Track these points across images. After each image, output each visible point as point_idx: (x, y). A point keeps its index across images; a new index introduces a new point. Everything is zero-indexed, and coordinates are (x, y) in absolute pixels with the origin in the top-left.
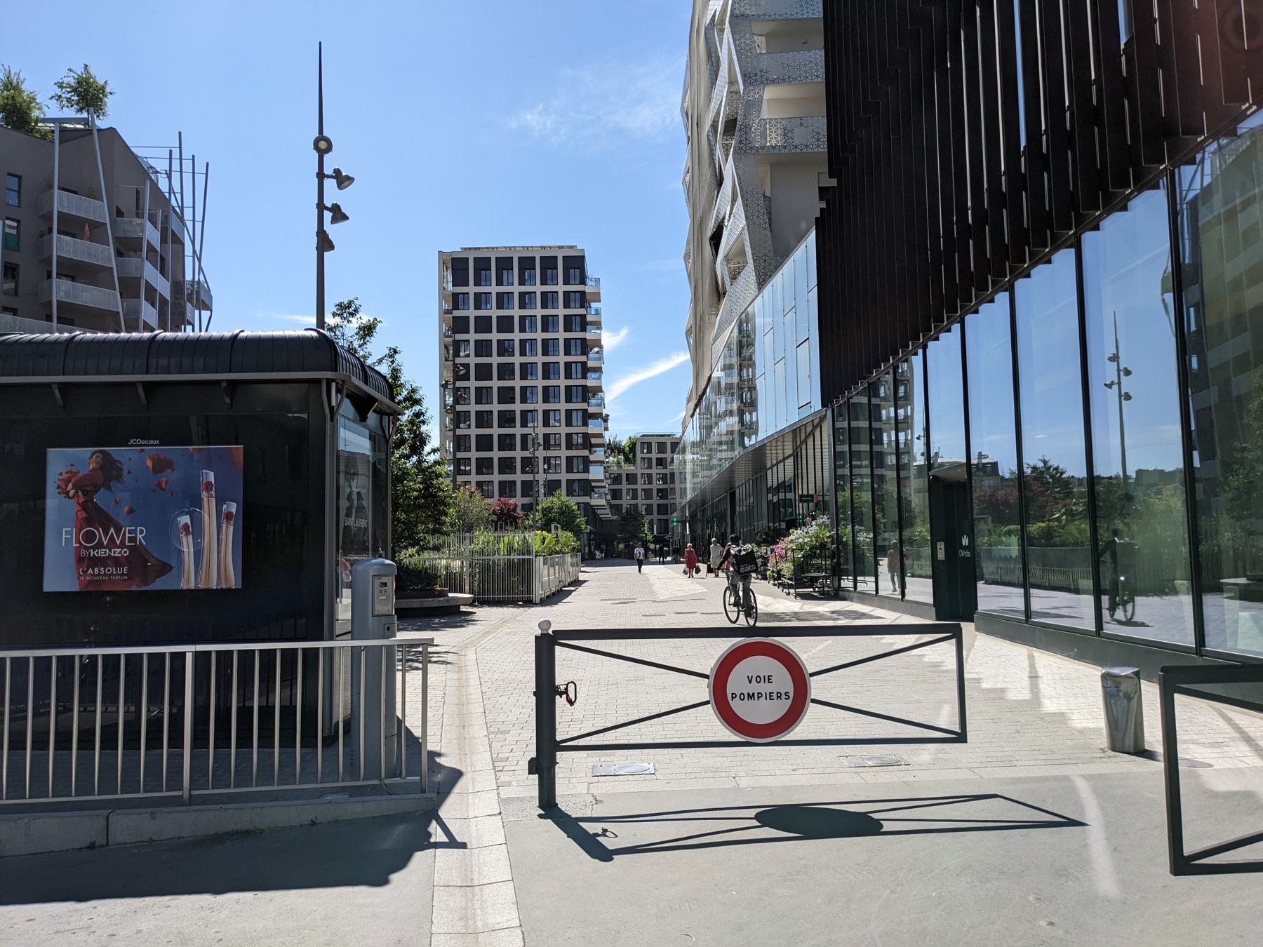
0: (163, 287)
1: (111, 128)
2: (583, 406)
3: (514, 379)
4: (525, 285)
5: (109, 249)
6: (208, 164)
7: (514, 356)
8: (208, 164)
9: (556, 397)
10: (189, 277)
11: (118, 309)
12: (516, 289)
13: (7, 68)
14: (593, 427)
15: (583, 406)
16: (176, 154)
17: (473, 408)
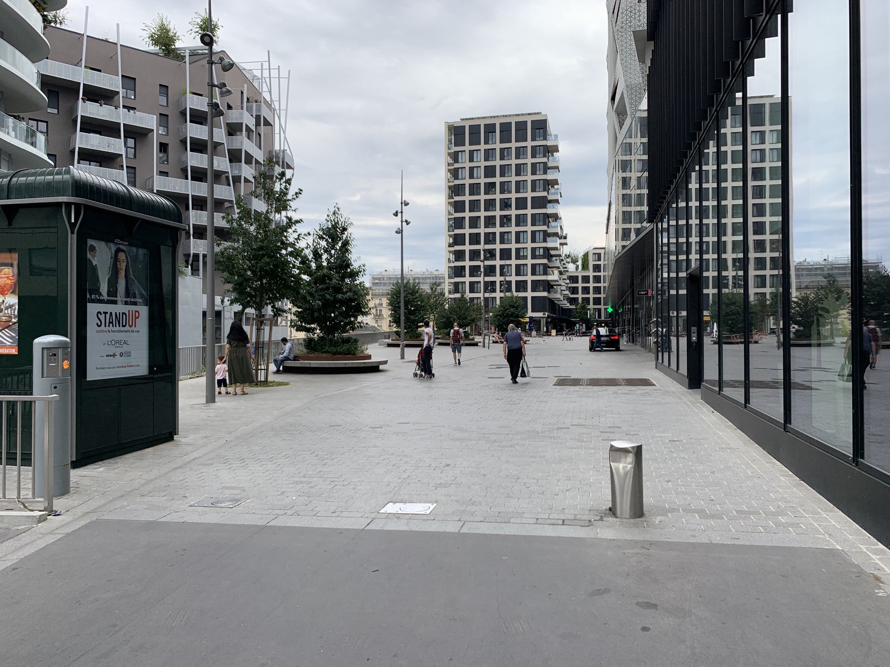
0: (259, 155)
1: (223, 51)
2: (545, 228)
3: (495, 211)
4: (504, 160)
6: (289, 71)
7: (495, 194)
8: (289, 71)
9: (525, 188)
10: (277, 148)
11: (223, 140)
12: (498, 146)
13: (161, 15)
14: (551, 243)
15: (545, 228)
16: (266, 65)
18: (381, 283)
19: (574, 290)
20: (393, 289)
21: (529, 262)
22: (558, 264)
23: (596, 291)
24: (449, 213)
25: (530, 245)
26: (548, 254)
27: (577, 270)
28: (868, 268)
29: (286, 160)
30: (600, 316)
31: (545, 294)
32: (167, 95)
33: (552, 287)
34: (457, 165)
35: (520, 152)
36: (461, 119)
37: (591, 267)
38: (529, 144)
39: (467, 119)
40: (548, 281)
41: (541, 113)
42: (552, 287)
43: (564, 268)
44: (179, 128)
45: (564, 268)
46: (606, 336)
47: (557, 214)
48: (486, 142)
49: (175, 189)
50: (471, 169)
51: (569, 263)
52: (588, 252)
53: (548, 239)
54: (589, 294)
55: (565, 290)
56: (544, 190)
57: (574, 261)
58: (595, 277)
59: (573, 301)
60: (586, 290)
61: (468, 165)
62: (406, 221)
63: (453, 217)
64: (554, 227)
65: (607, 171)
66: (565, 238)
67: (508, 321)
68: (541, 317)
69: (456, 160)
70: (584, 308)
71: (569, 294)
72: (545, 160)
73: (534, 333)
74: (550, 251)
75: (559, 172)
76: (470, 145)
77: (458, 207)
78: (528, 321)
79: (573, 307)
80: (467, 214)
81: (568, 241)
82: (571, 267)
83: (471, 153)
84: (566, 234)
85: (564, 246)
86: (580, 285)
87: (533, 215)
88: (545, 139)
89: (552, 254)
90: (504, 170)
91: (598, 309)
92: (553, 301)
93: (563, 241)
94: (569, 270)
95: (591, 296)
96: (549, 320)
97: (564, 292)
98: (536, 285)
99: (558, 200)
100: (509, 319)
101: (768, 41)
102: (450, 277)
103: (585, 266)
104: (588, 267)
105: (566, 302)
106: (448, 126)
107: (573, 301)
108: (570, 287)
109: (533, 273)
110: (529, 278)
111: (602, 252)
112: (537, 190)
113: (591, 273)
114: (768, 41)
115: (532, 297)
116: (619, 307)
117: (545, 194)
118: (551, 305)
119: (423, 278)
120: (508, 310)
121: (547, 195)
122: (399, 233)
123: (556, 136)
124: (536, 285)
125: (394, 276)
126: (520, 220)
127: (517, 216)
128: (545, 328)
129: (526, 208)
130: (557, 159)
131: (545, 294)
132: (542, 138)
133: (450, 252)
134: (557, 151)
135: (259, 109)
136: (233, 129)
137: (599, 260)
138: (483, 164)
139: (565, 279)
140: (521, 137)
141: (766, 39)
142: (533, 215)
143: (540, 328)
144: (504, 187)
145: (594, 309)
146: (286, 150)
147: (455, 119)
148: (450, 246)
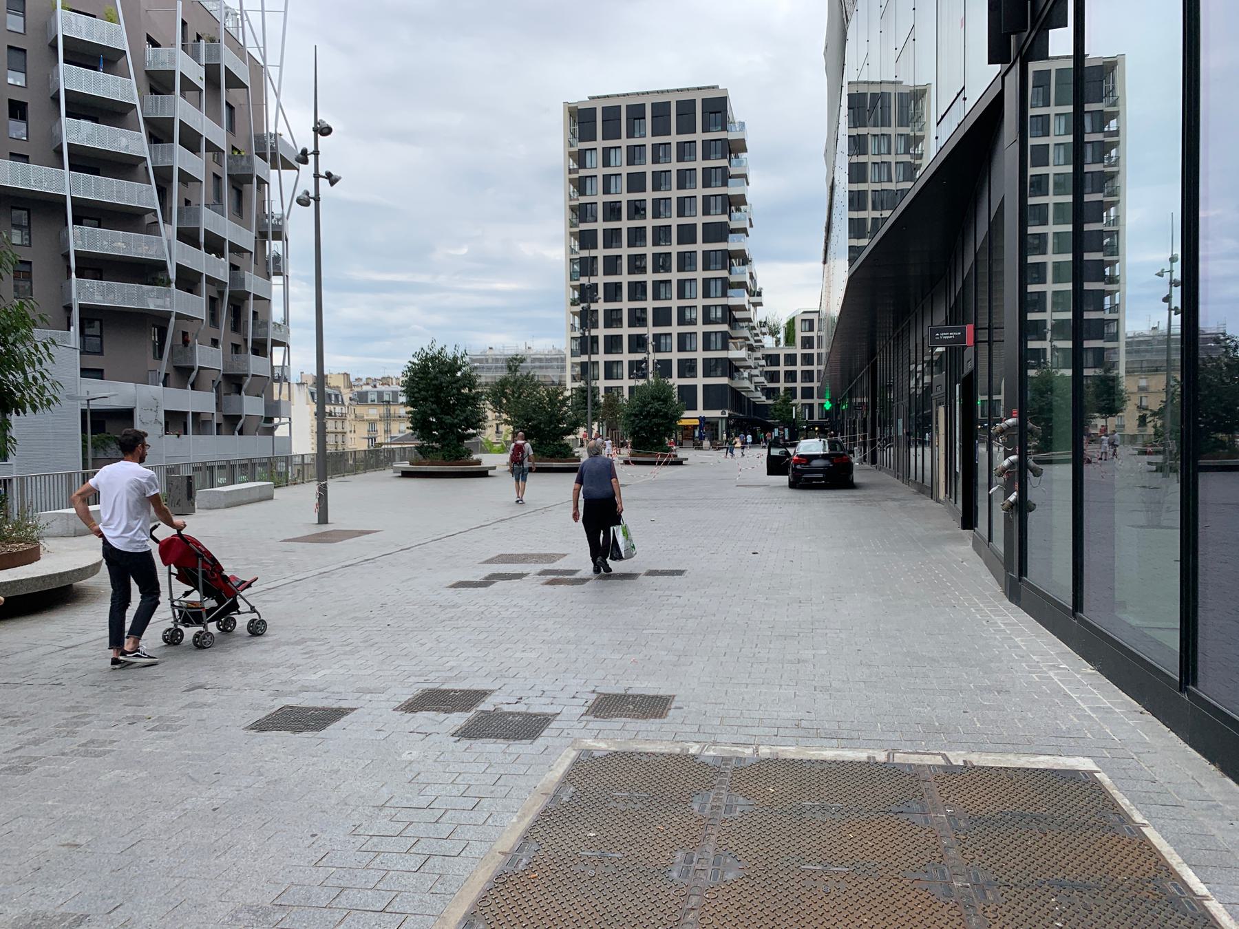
2: (724, 273)
4: (659, 163)
5: (130, 84)
11: (133, 99)
12: (649, 140)
14: (738, 298)
15: (724, 273)
17: (601, 332)
18: (483, 368)
19: (773, 377)
20: (414, 364)
21: (700, 329)
22: (746, 333)
23: (805, 378)
24: (572, 251)
25: (700, 302)
26: (729, 315)
27: (777, 345)
28: (1206, 340)
29: (280, 152)
30: (811, 416)
31: (724, 381)
32: (24, 12)
33: (737, 369)
34: (583, 173)
35: (684, 151)
36: (589, 98)
37: (798, 341)
38: (699, 137)
39: (598, 97)
40: (730, 361)
41: (717, 87)
42: (737, 369)
43: (756, 341)
44: (48, 75)
45: (756, 341)
46: (824, 457)
47: (744, 250)
48: (630, 135)
49: (28, 183)
50: (607, 178)
51: (764, 334)
52: (794, 318)
53: (730, 292)
54: (796, 381)
55: (757, 376)
56: (724, 212)
57: (774, 332)
58: (804, 356)
59: (769, 392)
60: (791, 376)
61: (601, 171)
62: (329, 175)
63: (577, 256)
64: (739, 273)
65: (825, 155)
66: (759, 294)
67: (650, 425)
68: (720, 418)
69: (582, 165)
70: (786, 402)
71: (766, 382)
72: (724, 163)
73: (706, 443)
74: (734, 312)
75: (748, 184)
76: (678, 244)
77: (586, 239)
78: (698, 423)
79: (771, 402)
80: (600, 252)
81: (764, 299)
82: (768, 341)
83: (606, 151)
84: (761, 289)
85: (758, 308)
86: (782, 368)
87: (706, 254)
88: (724, 129)
89: (736, 317)
90: (660, 180)
91: (809, 404)
92: (739, 393)
93: (755, 299)
94: (766, 346)
95: (799, 385)
96: (731, 422)
97: (756, 379)
98: (711, 367)
99: (746, 229)
100: (650, 421)
101: (1054, 34)
102: (573, 354)
103: (790, 340)
104: (794, 341)
105: (759, 394)
106: (569, 108)
107: (769, 392)
108: (766, 372)
109: (707, 347)
110: (700, 355)
111: (815, 317)
112: (712, 211)
113: (798, 351)
114: (1054, 34)
115: (704, 385)
116: (843, 400)
117: (724, 218)
118: (735, 398)
119: (547, 359)
120: (650, 406)
121: (728, 220)
122: (307, 204)
123: (742, 124)
124: (711, 367)
125: (502, 357)
126: (686, 261)
127: (681, 255)
128: (725, 435)
129: (695, 242)
130: (744, 164)
131: (724, 381)
132: (720, 128)
133: (574, 314)
134: (745, 150)
135: (214, 51)
136: (159, 83)
137: (811, 329)
138: (625, 170)
139: (759, 359)
140: (686, 126)
141: (1050, 31)
142: (706, 254)
143: (717, 434)
144: (659, 207)
145: (802, 404)
146: (281, 135)
147: (580, 96)
148: (573, 303)
